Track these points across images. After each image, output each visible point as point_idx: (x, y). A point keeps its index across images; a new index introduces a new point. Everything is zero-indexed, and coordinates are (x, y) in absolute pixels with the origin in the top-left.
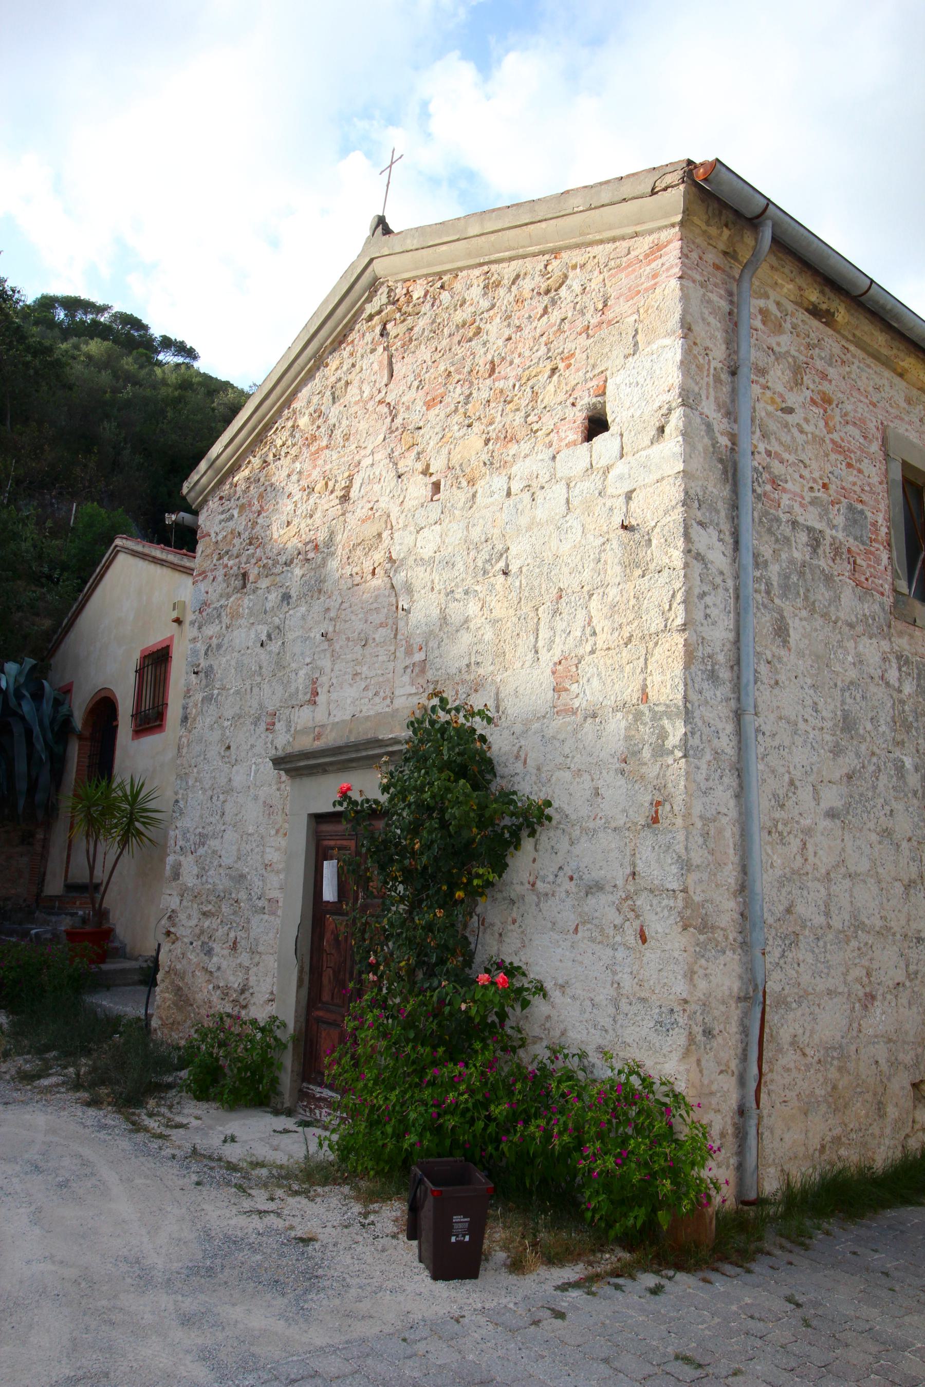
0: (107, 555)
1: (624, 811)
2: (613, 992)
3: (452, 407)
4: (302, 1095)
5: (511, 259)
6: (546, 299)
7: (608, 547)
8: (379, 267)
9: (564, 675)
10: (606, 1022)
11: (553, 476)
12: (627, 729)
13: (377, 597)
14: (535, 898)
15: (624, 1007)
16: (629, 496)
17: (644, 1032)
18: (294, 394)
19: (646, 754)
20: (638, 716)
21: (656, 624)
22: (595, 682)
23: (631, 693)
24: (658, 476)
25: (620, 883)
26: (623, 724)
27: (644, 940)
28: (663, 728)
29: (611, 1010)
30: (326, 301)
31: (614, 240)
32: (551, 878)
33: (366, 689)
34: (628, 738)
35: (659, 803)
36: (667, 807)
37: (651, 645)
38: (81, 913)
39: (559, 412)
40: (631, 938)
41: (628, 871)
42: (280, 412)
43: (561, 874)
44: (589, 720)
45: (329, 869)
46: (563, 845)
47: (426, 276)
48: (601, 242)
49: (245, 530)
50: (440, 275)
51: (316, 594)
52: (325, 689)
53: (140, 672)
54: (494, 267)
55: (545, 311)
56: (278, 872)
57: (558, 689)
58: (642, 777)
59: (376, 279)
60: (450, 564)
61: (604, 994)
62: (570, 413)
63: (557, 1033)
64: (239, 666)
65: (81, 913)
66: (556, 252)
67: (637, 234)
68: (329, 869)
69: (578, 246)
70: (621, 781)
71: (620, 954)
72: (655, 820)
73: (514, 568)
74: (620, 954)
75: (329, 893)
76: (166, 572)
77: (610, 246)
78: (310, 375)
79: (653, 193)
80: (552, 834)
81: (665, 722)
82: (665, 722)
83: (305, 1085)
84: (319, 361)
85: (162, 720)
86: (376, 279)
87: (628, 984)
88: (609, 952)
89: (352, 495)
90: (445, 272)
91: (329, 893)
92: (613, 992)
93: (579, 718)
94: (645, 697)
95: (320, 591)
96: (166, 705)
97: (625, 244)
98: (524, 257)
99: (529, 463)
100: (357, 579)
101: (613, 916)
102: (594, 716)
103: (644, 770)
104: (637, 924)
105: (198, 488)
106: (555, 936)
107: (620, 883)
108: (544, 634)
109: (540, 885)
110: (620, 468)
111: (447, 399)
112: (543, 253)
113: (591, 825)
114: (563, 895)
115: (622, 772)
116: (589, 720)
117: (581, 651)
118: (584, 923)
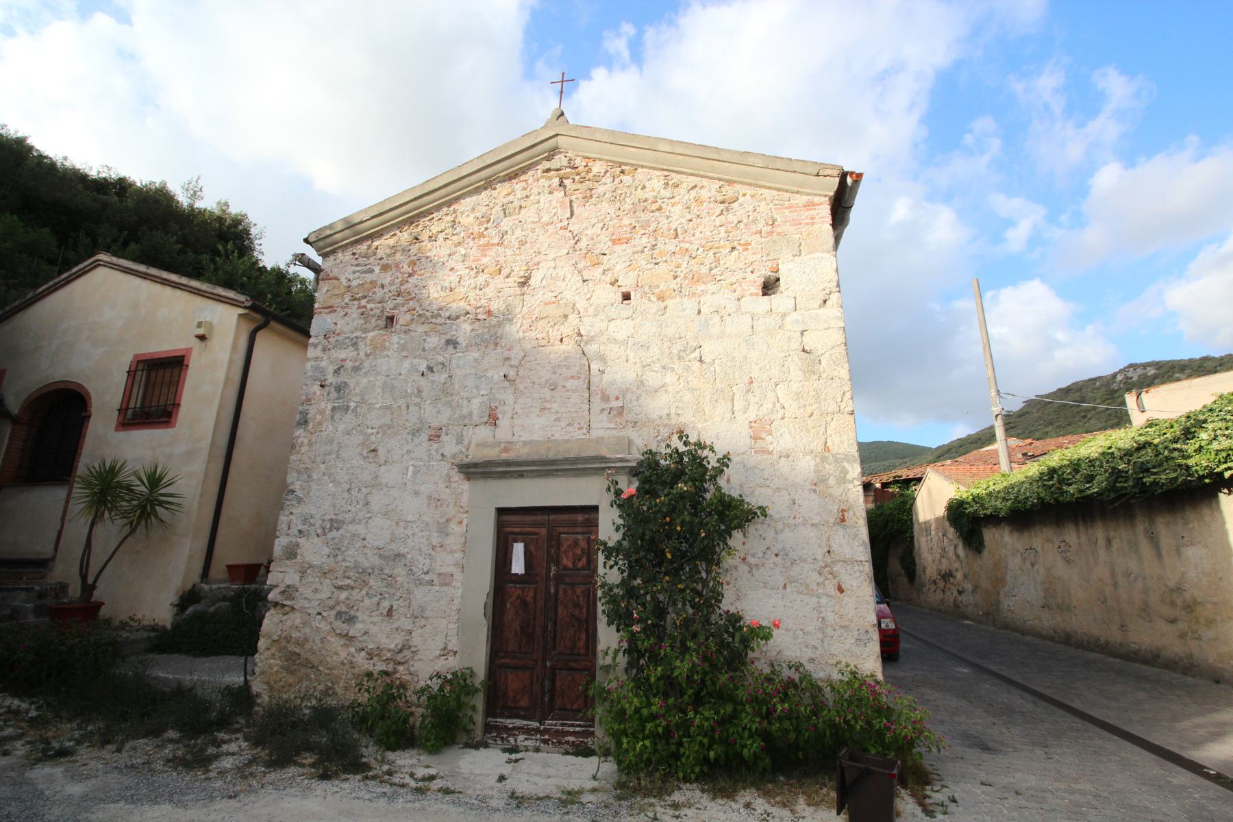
0: (86, 263)
1: (818, 514)
2: (819, 624)
3: (640, 248)
4: (488, 728)
5: (692, 175)
6: (722, 206)
7: (790, 359)
8: (561, 141)
9: (758, 430)
10: (817, 643)
11: (738, 309)
12: (817, 466)
13: (566, 358)
14: (747, 568)
15: (829, 631)
16: (802, 333)
17: (847, 647)
18: (457, 199)
19: (832, 481)
20: (823, 459)
21: (832, 407)
22: (787, 436)
23: (817, 446)
24: (826, 326)
25: (820, 557)
26: (812, 463)
27: (841, 590)
28: (844, 467)
29: (820, 635)
30: (506, 146)
31: (779, 190)
32: (760, 555)
33: (558, 420)
34: (816, 471)
35: (843, 511)
36: (851, 513)
37: (829, 419)
38: (37, 588)
39: (740, 275)
40: (832, 590)
41: (825, 550)
42: (438, 208)
43: (769, 552)
44: (783, 459)
45: (518, 550)
46: (770, 534)
47: (608, 161)
48: (769, 188)
49: (391, 284)
50: (620, 164)
51: (492, 346)
52: (508, 416)
53: (131, 373)
54: (673, 175)
55: (722, 213)
56: (452, 552)
57: (755, 438)
58: (831, 495)
59: (557, 148)
60: (645, 347)
61: (812, 626)
62: (750, 277)
63: (774, 653)
64: (388, 388)
65: (37, 588)
66: (730, 182)
67: (798, 192)
68: (518, 550)
69: (750, 185)
70: (813, 496)
71: (824, 600)
72: (843, 520)
73: (707, 359)
74: (824, 600)
75: (518, 567)
76: (168, 291)
77: (775, 192)
78: (477, 191)
79: (818, 175)
80: (759, 526)
81: (846, 465)
82: (846, 465)
83: (490, 719)
84: (489, 184)
85: (170, 417)
86: (557, 148)
87: (831, 618)
88: (815, 600)
89: (531, 282)
90: (627, 164)
91: (518, 567)
92: (819, 624)
93: (775, 456)
94: (826, 449)
95: (496, 345)
96: (177, 405)
97: (787, 195)
98: (702, 177)
99: (715, 297)
100: (544, 342)
101: (814, 576)
102: (788, 456)
103: (831, 490)
104: (835, 582)
105: (329, 240)
106: (768, 591)
107: (820, 557)
108: (739, 405)
109: (750, 559)
110: (795, 316)
111: (633, 242)
112: (720, 180)
113: (792, 522)
114: (772, 565)
115: (815, 491)
116: (783, 459)
117: (774, 417)
118: (790, 582)
